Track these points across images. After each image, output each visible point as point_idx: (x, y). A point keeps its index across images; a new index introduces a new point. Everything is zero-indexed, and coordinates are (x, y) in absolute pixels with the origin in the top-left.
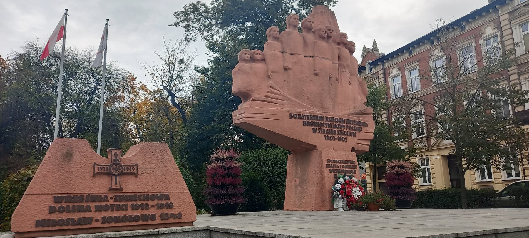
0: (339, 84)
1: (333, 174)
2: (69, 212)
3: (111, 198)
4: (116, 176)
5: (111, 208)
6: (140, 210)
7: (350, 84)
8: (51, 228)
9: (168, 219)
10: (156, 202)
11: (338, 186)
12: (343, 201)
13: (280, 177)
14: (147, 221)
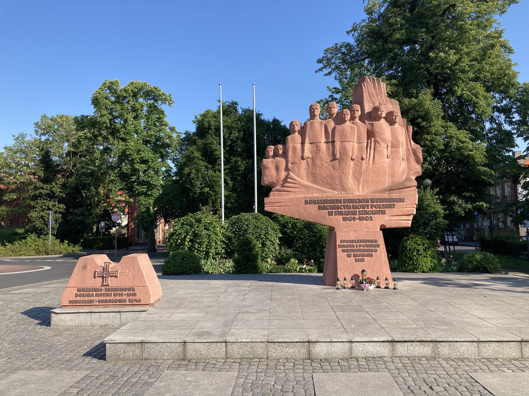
3: (104, 290)
5: (103, 295)
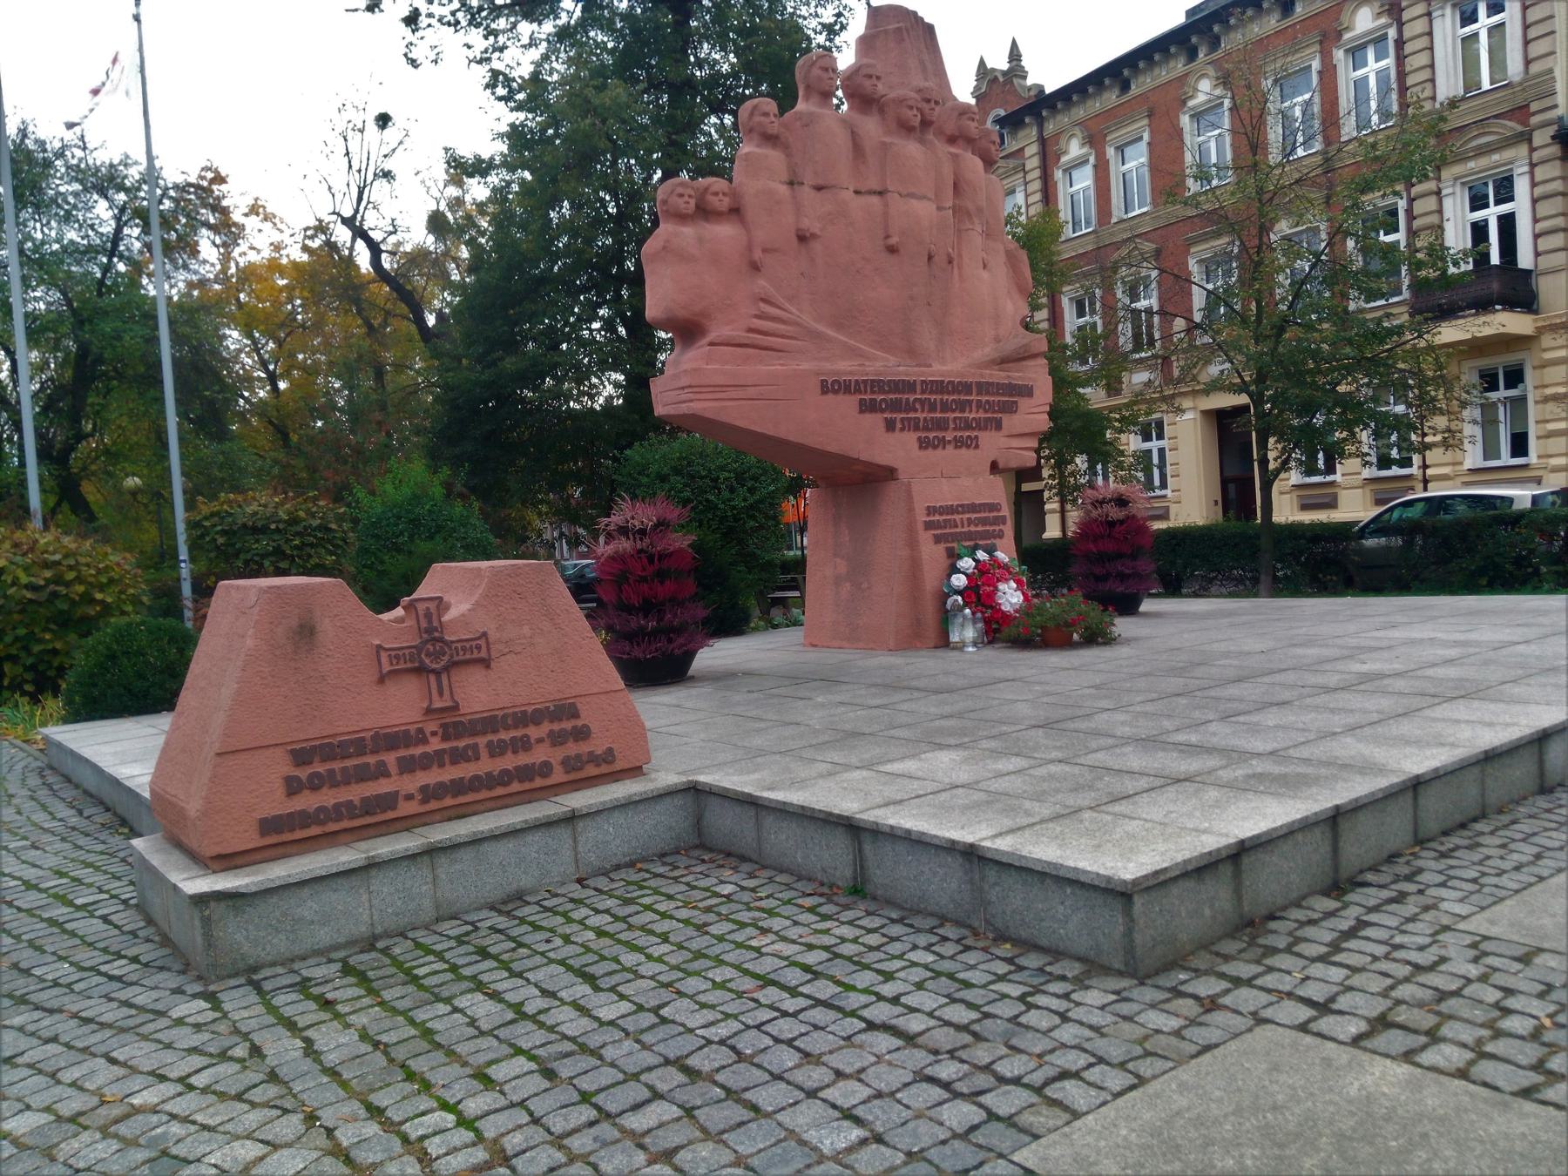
0: (956, 271)
1: (942, 547)
2: (335, 785)
3: (434, 734)
4: (437, 673)
5: (438, 759)
6: (509, 753)
7: (985, 267)
8: (299, 834)
9: (581, 769)
10: (546, 727)
11: (959, 581)
12: (974, 622)
13: (753, 517)
14: (531, 780)
